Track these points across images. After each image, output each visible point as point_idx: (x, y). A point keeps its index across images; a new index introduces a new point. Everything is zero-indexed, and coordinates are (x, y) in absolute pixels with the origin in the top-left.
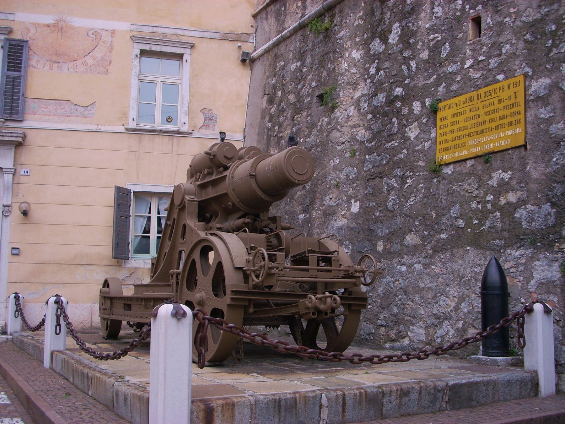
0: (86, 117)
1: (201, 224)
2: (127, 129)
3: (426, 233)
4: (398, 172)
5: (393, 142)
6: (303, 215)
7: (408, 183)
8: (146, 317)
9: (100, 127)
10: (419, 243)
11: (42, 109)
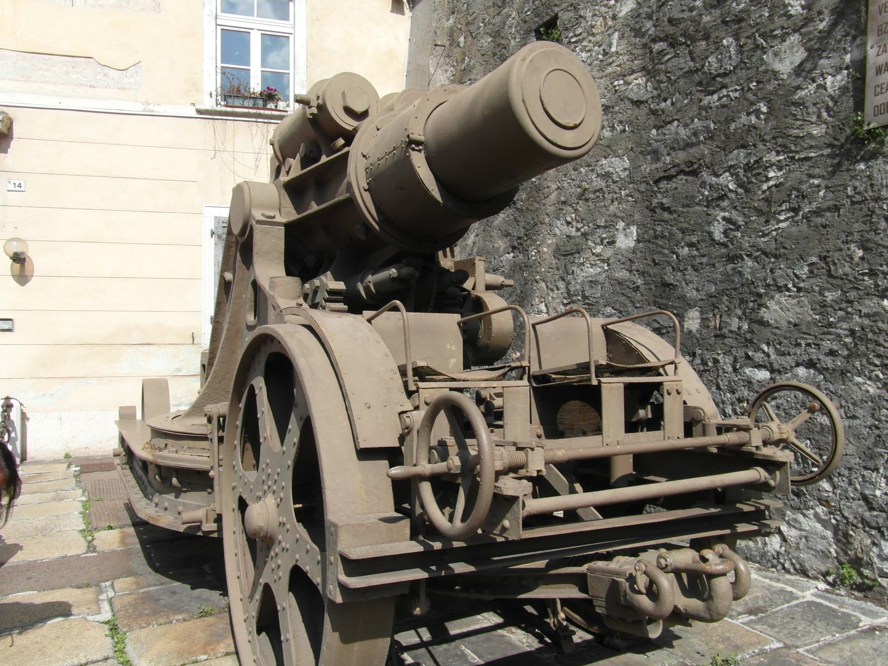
0: (124, 89)
1: (295, 281)
2: (199, 112)
3: (830, 296)
4: (739, 157)
5: (724, 92)
6: (512, 255)
7: (768, 179)
8: (166, 509)
9: (151, 107)
10: (809, 319)
11: (40, 72)
